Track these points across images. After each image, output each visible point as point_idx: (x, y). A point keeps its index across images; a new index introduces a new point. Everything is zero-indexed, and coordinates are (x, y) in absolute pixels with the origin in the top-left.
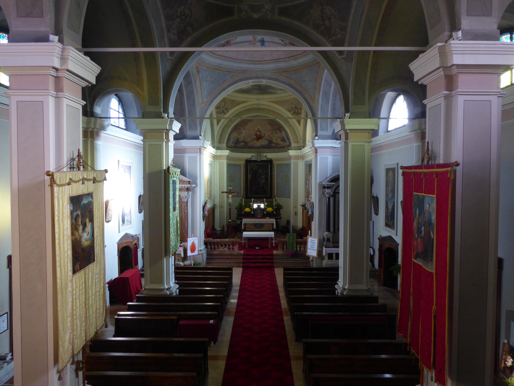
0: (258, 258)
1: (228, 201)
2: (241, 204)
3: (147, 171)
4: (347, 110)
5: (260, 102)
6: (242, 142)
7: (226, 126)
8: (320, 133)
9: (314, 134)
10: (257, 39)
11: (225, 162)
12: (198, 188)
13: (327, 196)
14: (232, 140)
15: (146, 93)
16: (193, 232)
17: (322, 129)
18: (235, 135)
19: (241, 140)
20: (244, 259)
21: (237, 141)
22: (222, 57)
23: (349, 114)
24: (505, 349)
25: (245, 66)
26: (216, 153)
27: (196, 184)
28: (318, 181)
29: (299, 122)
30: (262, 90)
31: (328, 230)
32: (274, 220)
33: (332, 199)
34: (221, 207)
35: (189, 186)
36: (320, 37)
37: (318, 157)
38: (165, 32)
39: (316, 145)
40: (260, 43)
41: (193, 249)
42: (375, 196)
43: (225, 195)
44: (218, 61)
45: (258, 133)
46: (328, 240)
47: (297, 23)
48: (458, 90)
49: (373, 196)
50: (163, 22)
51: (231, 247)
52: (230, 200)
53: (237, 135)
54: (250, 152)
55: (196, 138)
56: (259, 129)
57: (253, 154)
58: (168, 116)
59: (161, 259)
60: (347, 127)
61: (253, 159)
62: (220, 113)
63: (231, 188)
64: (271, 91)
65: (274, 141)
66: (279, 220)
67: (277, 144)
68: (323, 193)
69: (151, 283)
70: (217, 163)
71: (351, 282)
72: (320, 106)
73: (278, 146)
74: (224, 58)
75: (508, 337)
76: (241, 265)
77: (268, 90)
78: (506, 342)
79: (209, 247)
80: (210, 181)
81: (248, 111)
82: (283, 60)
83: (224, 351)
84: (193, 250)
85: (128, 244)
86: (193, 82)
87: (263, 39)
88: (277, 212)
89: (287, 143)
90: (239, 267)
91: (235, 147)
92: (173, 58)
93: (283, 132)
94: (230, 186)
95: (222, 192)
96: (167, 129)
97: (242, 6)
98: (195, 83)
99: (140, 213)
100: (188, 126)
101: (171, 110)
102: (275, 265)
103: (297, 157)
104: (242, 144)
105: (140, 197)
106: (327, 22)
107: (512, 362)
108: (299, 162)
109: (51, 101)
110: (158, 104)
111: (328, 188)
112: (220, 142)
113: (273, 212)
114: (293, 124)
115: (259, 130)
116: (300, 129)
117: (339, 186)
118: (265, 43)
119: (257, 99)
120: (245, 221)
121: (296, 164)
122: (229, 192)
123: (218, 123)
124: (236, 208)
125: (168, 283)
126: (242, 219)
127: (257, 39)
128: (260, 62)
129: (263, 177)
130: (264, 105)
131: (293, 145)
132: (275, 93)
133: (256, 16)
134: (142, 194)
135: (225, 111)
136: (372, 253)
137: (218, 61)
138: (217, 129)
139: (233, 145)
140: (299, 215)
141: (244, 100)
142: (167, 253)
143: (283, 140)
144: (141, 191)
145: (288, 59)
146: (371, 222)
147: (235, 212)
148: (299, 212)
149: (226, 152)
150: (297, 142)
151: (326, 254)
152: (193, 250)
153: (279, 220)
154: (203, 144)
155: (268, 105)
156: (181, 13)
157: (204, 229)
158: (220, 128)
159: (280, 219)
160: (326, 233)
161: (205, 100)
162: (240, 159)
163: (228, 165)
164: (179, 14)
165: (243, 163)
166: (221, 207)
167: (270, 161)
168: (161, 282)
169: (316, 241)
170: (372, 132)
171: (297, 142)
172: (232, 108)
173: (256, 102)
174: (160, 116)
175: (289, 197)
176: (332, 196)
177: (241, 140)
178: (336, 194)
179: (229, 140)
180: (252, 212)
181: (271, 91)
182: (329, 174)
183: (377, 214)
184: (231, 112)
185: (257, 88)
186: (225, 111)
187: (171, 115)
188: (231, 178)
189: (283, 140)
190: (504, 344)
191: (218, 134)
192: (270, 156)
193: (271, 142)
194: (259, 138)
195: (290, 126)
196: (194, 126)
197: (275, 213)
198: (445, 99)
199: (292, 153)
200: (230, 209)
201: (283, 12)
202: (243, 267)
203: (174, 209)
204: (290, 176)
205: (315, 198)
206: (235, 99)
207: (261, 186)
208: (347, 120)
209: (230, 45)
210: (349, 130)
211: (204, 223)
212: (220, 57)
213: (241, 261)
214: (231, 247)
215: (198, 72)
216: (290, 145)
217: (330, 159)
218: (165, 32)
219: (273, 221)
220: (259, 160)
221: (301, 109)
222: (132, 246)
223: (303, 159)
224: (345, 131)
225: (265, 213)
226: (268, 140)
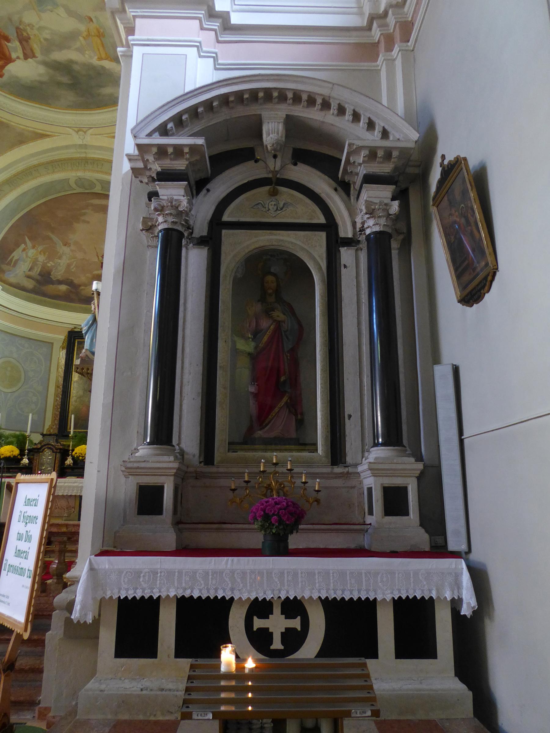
6: (60, 282)
19: (58, 274)
136: (469, 603)
141: (40, 128)
173: (76, 139)
197: (25, 461)
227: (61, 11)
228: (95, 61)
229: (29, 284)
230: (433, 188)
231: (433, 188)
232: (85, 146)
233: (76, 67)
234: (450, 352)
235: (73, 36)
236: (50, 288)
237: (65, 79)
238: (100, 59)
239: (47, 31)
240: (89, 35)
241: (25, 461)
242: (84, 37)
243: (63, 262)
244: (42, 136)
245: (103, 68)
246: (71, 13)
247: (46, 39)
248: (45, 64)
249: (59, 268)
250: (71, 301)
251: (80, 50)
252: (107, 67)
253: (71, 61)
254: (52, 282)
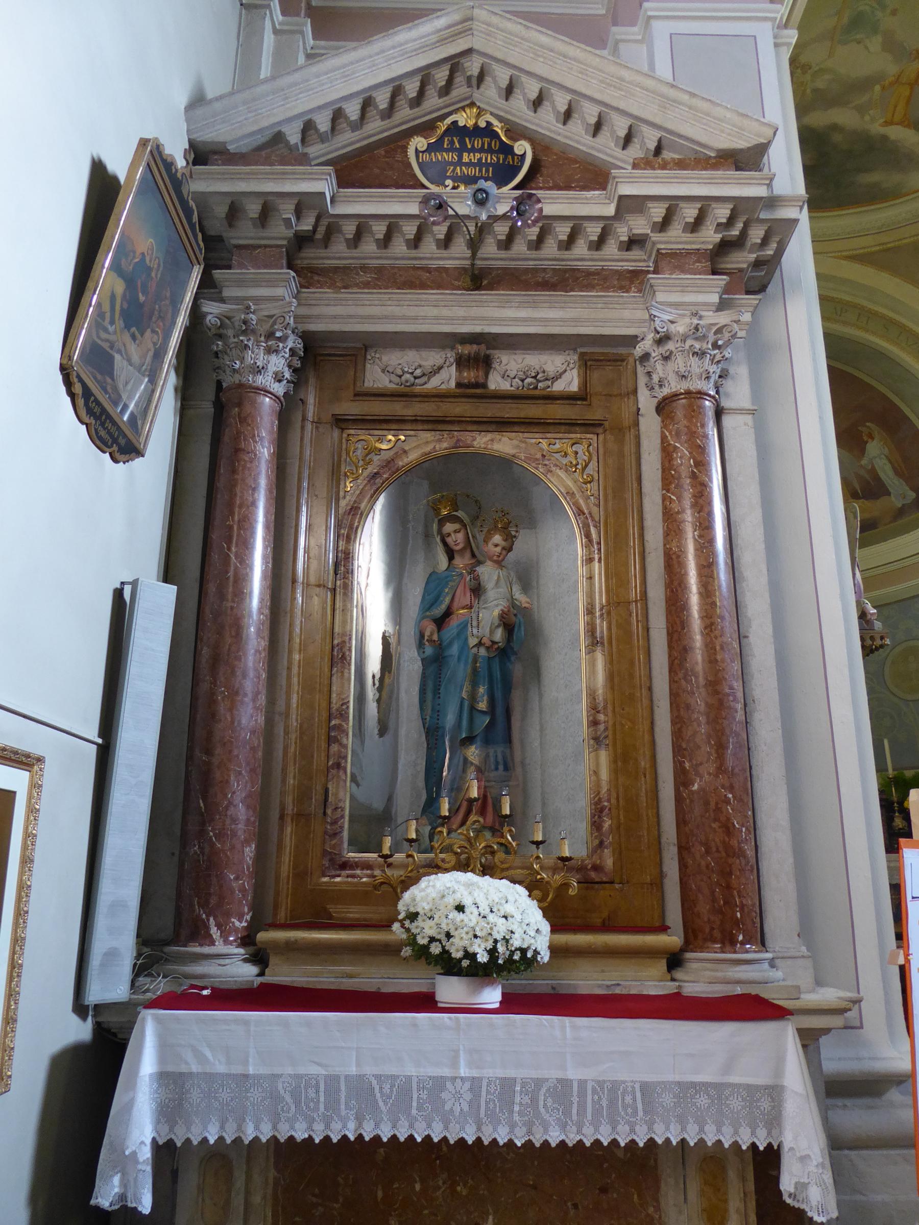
227: (875, 43)
228: (877, 128)
233: (837, 138)
235: (865, 84)
238: (887, 123)
239: (827, 77)
240: (897, 81)
242: (883, 88)
245: (885, 138)
246: (891, 45)
247: (815, 90)
251: (861, 110)
252: (893, 137)
253: (835, 127)
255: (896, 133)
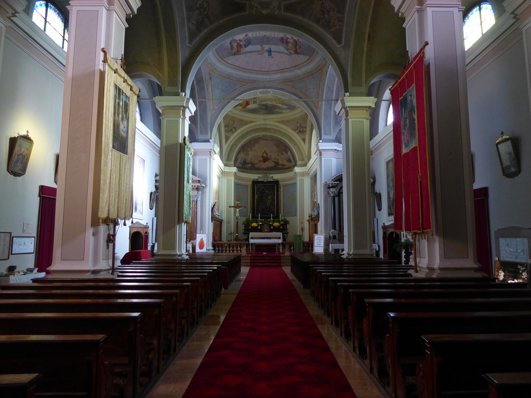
0: (264, 256)
1: (235, 215)
2: (248, 220)
3: (164, 144)
4: (346, 91)
5: (267, 122)
6: (249, 163)
7: (234, 145)
8: (323, 137)
9: (319, 138)
10: (265, 49)
11: (232, 179)
12: (208, 189)
13: (332, 195)
14: (239, 160)
15: (166, 75)
16: (202, 229)
17: (326, 134)
18: (242, 156)
19: (248, 161)
20: (251, 260)
21: (244, 163)
22: (232, 66)
23: (348, 94)
24: (497, 266)
25: (253, 76)
26: (224, 169)
27: (206, 184)
28: (323, 182)
29: (304, 140)
30: (268, 109)
31: (334, 228)
32: (281, 234)
33: (337, 199)
34: (228, 223)
35: (199, 185)
36: (321, 29)
37: (323, 159)
38: (186, 21)
39: (320, 148)
40: (267, 53)
41: (201, 246)
42: (378, 192)
43: (232, 209)
44: (229, 70)
45: (265, 155)
46: (334, 237)
47: (300, 18)
48: (427, 3)
49: (376, 193)
50: (185, 11)
51: (239, 248)
52: (237, 214)
53: (244, 156)
54: (257, 173)
55: (208, 141)
56: (265, 151)
57: (260, 175)
58: (185, 95)
59: (174, 226)
60: (347, 104)
61: (260, 180)
62: (229, 131)
63: (238, 203)
64: (277, 110)
65: (280, 162)
66: (285, 235)
67: (283, 165)
68: (328, 193)
69: (163, 249)
70: (225, 180)
71: (355, 248)
72: (323, 112)
73: (284, 167)
74: (234, 67)
75: (498, 255)
76: (249, 264)
77: (275, 110)
78: (497, 259)
79: (217, 249)
80: (218, 193)
81: (256, 130)
82: (289, 70)
83: (233, 298)
84: (201, 247)
85: (140, 230)
86: (206, 88)
87: (270, 48)
88: (283, 227)
89: (293, 163)
90: (247, 266)
91: (242, 168)
92: (191, 46)
93: (289, 153)
94: (238, 201)
95: (230, 207)
96: (184, 107)
97: (253, 3)
98: (208, 89)
99: (151, 209)
100: (199, 131)
101: (188, 91)
102: (282, 264)
103: (303, 174)
104: (249, 165)
105: (151, 194)
106: (326, 16)
107: (504, 276)
108: (305, 179)
109: (104, 11)
110: (176, 85)
111: (333, 187)
112: (228, 159)
113: (279, 227)
114: (298, 143)
115: (265, 152)
116: (305, 147)
117: (342, 187)
118: (272, 53)
119: (264, 120)
120: (252, 234)
121: (302, 181)
122: (236, 207)
123: (226, 142)
124: (243, 224)
125: (180, 249)
126: (249, 234)
127: (265, 49)
128: (267, 72)
129: (269, 197)
130: (270, 125)
131: (299, 162)
132: (281, 113)
133: (265, 12)
134: (158, 173)
135: (233, 130)
136: (377, 249)
137: (229, 70)
138: (225, 147)
139: (240, 166)
140: (305, 231)
142: (180, 220)
143: (289, 161)
144: (156, 170)
145: (293, 69)
146: (375, 219)
147: (242, 227)
148: (305, 227)
149: (234, 169)
150: (303, 160)
151: (332, 249)
152: (201, 247)
153: (285, 235)
154: (213, 147)
155: (274, 125)
156: (200, 5)
157: (212, 231)
158: (228, 146)
159: (287, 233)
160: (332, 231)
161: (216, 107)
162: (247, 180)
163: (236, 184)
164: (198, 6)
165: (250, 183)
166: (228, 223)
167: (277, 182)
168: (174, 248)
169: (322, 238)
170: (370, 110)
171: (303, 160)
172: (240, 128)
173: (263, 122)
174: (178, 94)
175: (296, 215)
176: (337, 196)
177: (248, 161)
178: (340, 194)
179: (236, 159)
180: (259, 227)
181: (277, 110)
182: (334, 173)
183: (380, 210)
184: (239, 131)
185: (264, 108)
186: (233, 130)
187: (188, 95)
188: (237, 197)
189: (289, 161)
190: (495, 261)
191: (226, 150)
192: (277, 176)
193: (277, 164)
194: (265, 160)
195: (296, 145)
196: (205, 131)
197: (281, 227)
198: (418, 13)
199: (297, 169)
200: (237, 223)
201: (289, 8)
202: (251, 266)
203: (188, 182)
204: (296, 194)
205: (320, 199)
206: (243, 118)
207: (268, 206)
208: (346, 99)
209: (240, 54)
210: (349, 107)
211: (212, 224)
212: (230, 66)
213: (249, 261)
214: (239, 248)
215: (211, 78)
216: (296, 162)
217: (334, 161)
218: (186, 21)
219: (280, 234)
220: (265, 181)
221: (306, 128)
222: (143, 232)
223: (308, 175)
224: (345, 108)
225: (272, 227)
226: (273, 162)
228: (275, 104)
229: (240, 166)
230: (331, 334)
231: (331, 334)
232: (266, 124)
234: (377, 217)
236: (246, 166)
237: (264, 108)
241: (281, 227)
243: (250, 157)
244: (252, 122)
248: (259, 104)
249: (249, 158)
250: (252, 170)
254: (246, 164)
255: (278, 105)
